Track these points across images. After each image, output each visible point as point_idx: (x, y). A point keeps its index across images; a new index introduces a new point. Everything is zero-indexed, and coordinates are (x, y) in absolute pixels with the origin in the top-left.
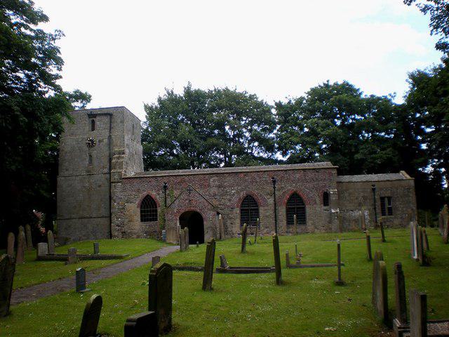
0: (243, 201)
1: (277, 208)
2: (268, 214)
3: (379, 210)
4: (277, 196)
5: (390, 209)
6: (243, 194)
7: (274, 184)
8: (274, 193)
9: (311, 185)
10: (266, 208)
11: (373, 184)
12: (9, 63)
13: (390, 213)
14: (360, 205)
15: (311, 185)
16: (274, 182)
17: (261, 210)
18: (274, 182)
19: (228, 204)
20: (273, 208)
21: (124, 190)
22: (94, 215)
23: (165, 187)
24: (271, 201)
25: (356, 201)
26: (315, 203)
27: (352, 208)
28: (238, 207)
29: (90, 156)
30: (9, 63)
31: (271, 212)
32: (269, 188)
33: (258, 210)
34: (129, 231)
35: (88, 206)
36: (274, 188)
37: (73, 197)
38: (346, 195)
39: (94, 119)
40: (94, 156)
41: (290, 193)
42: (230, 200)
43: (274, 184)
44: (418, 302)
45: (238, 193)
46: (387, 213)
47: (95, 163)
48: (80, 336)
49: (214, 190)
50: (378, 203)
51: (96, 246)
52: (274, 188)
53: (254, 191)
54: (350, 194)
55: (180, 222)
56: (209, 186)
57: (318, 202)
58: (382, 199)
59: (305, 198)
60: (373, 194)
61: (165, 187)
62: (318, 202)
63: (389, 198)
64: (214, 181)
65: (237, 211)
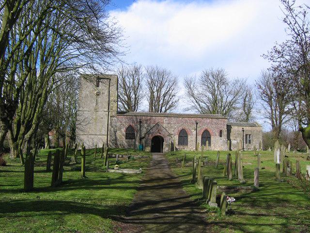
3: (245, 141)
5: (250, 141)
6: (180, 129)
12: (117, 167)
13: (250, 143)
16: (197, 123)
17: (189, 137)
22: (98, 134)
23: (141, 122)
24: (194, 132)
30: (117, 167)
31: (194, 138)
41: (204, 129)
46: (80, 165)
47: (100, 105)
50: (245, 138)
51: (259, 211)
53: (187, 128)
55: (12, 212)
57: (217, 135)
58: (246, 135)
59: (211, 132)
61: (141, 122)
62: (217, 135)
63: (250, 135)
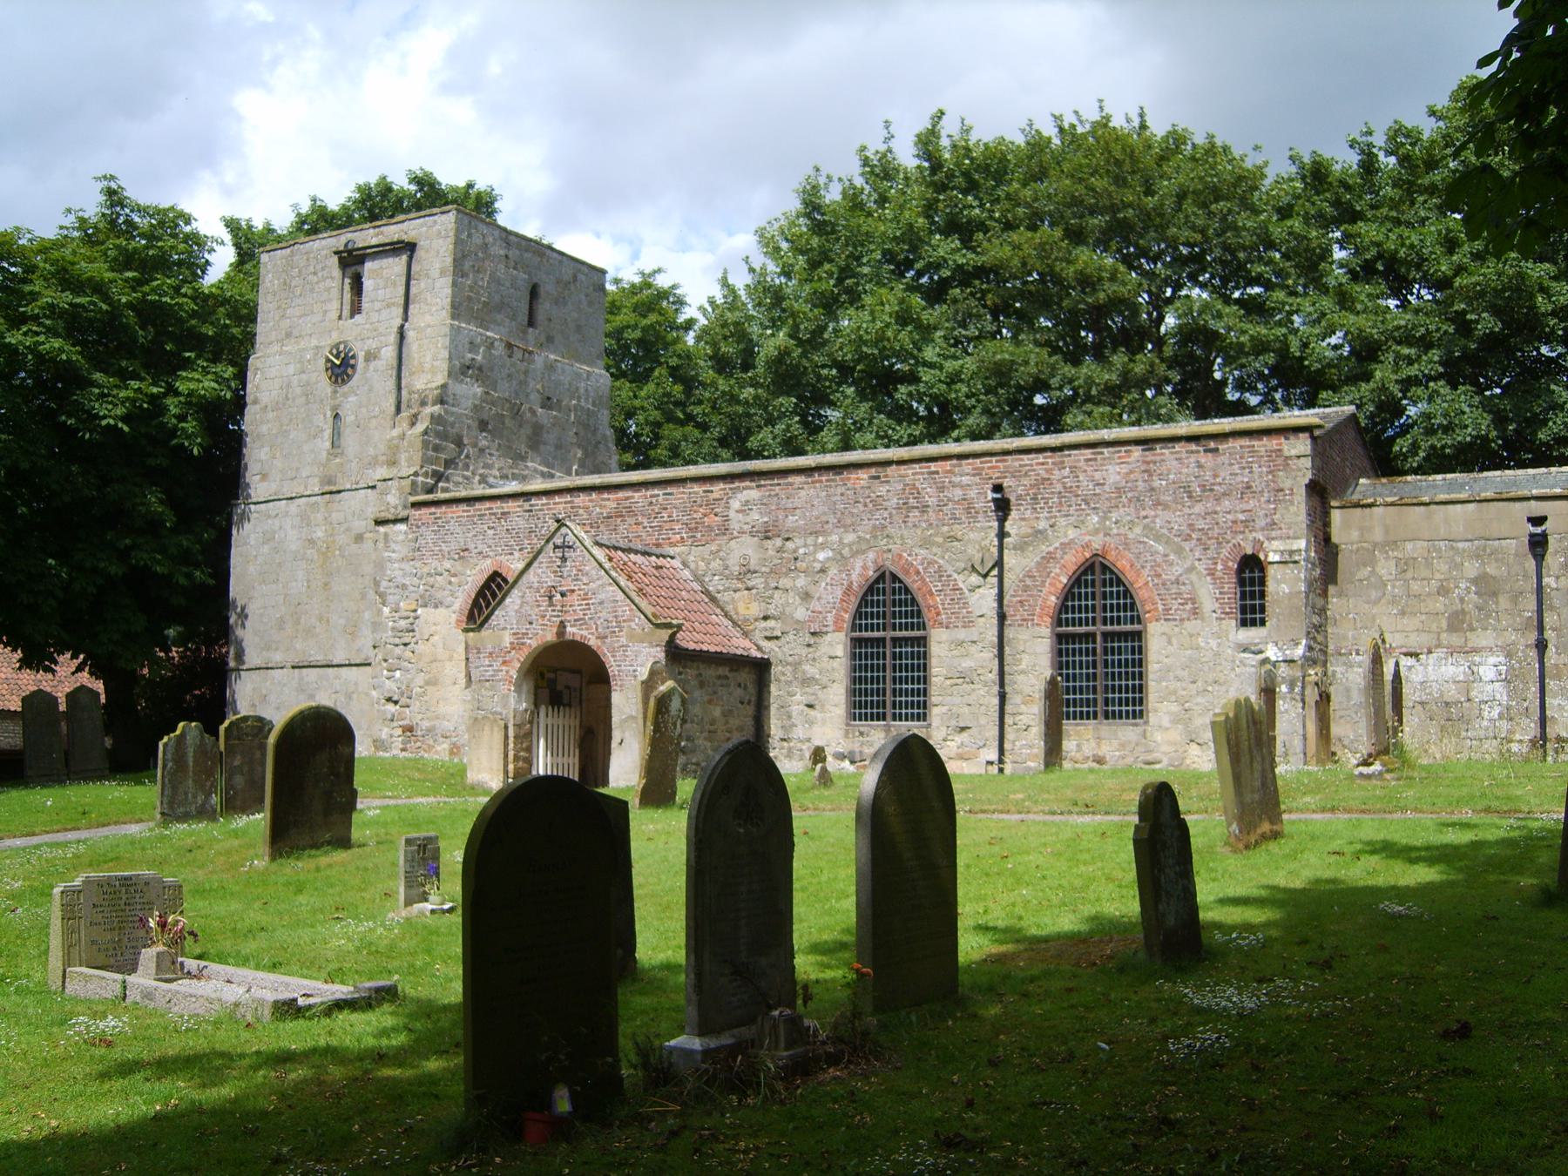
0: (863, 602)
1: (1009, 633)
2: (967, 664)
4: (1008, 577)
6: (861, 570)
7: (1002, 521)
8: (999, 563)
9: (1178, 520)
10: (961, 634)
11: (1537, 508)
14: (1457, 622)
15: (1178, 520)
16: (1002, 507)
18: (1002, 507)
19: (801, 613)
20: (992, 635)
21: (416, 553)
24: (984, 600)
25: (1439, 604)
26: (1195, 612)
27: (1414, 641)
28: (838, 630)
29: (336, 416)
32: (981, 536)
33: (922, 641)
34: (426, 724)
35: (320, 619)
36: (1002, 535)
37: (276, 581)
38: (1386, 568)
39: (358, 268)
40: (349, 418)
42: (806, 596)
43: (1002, 521)
44: (291, 1025)
45: (841, 560)
46: (1136, 627)
48: (8, 1145)
49: (744, 549)
52: (1002, 535)
54: (1405, 565)
56: (725, 530)
59: (1141, 583)
60: (1531, 564)
62: (1208, 603)
64: (746, 508)
65: (837, 645)
